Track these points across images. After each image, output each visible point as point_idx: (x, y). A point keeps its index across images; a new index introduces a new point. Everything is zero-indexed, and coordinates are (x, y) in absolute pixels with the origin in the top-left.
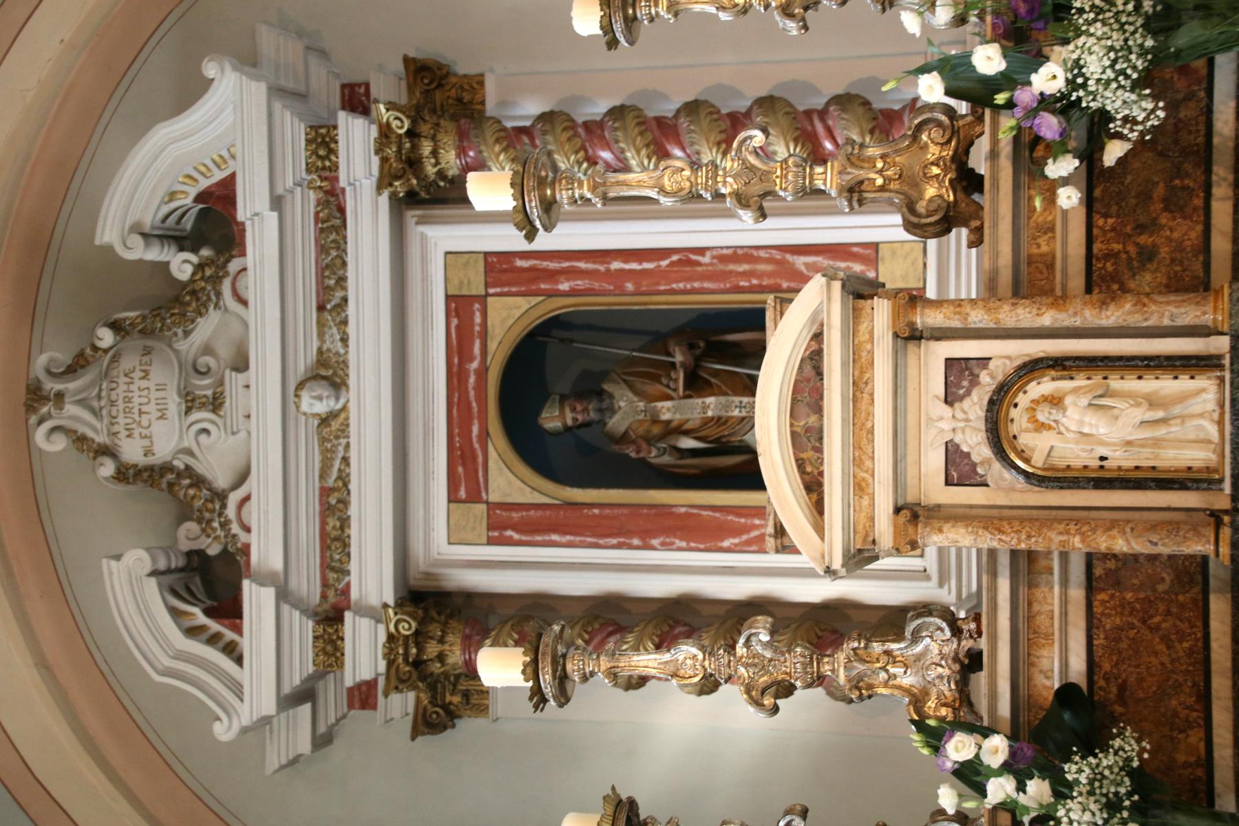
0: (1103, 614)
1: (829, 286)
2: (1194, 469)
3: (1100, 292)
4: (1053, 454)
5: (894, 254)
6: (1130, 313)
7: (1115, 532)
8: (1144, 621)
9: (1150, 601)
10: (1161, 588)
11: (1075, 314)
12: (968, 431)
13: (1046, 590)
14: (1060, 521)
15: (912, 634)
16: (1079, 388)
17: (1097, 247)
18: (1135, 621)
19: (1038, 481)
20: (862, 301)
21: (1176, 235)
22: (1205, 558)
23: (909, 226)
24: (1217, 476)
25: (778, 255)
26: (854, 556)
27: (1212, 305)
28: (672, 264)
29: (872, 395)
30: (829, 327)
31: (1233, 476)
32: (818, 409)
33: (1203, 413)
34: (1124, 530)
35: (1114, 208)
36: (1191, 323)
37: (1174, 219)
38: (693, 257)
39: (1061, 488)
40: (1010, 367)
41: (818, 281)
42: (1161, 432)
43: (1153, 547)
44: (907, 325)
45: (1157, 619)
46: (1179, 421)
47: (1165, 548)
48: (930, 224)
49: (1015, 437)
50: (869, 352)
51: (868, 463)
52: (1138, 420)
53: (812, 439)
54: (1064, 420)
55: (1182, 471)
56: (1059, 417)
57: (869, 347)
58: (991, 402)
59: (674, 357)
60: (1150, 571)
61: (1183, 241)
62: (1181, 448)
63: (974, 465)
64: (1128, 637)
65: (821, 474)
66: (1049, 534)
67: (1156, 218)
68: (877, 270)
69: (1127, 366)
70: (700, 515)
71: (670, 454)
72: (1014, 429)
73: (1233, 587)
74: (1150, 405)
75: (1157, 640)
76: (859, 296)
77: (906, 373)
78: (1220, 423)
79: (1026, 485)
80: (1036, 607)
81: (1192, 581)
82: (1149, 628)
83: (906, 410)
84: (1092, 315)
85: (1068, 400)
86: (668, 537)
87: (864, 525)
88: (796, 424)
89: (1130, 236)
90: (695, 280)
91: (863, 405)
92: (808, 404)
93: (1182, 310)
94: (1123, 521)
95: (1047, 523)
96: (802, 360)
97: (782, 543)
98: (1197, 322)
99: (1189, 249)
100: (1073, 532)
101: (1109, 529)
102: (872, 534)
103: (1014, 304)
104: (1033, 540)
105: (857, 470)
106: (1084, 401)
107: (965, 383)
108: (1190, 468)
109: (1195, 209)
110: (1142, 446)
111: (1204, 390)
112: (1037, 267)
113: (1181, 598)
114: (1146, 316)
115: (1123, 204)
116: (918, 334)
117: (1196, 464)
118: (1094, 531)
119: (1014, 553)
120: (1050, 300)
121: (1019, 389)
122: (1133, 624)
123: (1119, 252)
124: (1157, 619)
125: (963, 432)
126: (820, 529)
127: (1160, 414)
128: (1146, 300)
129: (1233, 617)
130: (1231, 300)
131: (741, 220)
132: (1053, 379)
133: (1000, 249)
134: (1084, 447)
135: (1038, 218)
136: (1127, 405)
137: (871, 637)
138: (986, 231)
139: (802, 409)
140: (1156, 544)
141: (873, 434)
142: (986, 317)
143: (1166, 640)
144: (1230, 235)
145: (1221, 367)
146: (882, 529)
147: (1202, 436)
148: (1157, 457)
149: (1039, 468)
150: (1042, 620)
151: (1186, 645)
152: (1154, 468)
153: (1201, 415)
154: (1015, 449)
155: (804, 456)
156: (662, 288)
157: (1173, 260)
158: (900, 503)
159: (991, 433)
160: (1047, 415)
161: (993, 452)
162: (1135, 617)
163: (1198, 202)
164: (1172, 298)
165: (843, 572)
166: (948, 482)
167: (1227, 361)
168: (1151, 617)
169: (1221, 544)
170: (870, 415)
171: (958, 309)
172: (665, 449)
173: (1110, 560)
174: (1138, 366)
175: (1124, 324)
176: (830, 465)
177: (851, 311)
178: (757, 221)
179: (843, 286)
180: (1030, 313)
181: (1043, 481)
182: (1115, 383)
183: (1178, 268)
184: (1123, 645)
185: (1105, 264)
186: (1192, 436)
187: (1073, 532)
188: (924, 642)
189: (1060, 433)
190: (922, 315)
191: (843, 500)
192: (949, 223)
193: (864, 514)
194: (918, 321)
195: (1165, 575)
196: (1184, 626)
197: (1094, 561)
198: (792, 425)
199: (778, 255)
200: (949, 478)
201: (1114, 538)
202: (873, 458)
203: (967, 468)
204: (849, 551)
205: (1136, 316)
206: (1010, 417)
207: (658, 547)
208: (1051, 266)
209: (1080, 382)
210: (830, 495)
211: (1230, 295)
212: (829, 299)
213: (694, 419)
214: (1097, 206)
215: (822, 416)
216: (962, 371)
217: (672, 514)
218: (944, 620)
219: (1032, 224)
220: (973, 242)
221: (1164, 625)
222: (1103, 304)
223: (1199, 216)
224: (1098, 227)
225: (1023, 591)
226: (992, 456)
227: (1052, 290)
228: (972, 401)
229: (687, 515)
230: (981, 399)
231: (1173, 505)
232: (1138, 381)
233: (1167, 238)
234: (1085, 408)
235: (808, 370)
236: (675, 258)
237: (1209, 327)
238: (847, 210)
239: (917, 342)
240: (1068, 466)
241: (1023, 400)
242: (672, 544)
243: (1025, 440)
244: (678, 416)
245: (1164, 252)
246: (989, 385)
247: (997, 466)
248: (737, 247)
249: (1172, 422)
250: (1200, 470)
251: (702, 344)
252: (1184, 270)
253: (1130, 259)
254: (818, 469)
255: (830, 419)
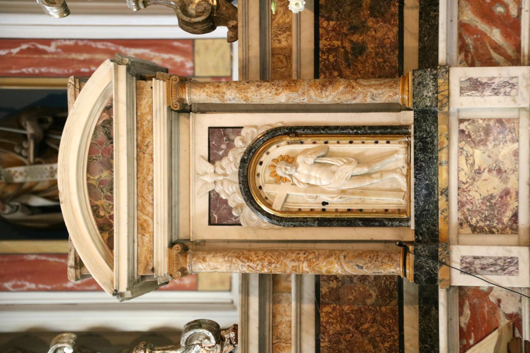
0: (327, 322)
1: (116, 70)
2: (390, 211)
3: (325, 78)
4: (288, 200)
5: (207, 48)
6: (343, 93)
7: (332, 259)
8: (357, 328)
9: (361, 312)
10: (369, 302)
11: (303, 93)
12: (225, 183)
13: (286, 305)
14: (293, 251)
15: (186, 343)
16: (308, 150)
17: (322, 43)
18: (351, 328)
19: (278, 221)
20: (144, 82)
21: (379, 35)
22: (400, 279)
23: (184, 25)
24: (405, 217)
25: (112, 47)
26: (138, 281)
27: (401, 87)
28: (22, 52)
29: (152, 155)
30: (117, 102)
31: (415, 216)
32: (109, 167)
33: (396, 169)
34: (339, 257)
35: (334, 14)
36: (387, 102)
37: (378, 22)
38: (40, 47)
39: (295, 226)
40: (258, 134)
41: (107, 66)
42: (366, 183)
43: (360, 270)
44: (178, 101)
45: (366, 326)
46: (378, 175)
47: (370, 271)
48: (198, 23)
49: (260, 187)
50: (149, 122)
51: (149, 208)
52: (349, 174)
53: (104, 190)
54: (296, 175)
55: (381, 213)
56: (293, 172)
57: (149, 118)
58: (243, 161)
59: (25, 130)
60: (361, 289)
61: (384, 39)
62: (380, 195)
63: (230, 209)
64: (345, 340)
65: (112, 217)
66: (285, 261)
67: (365, 22)
68: (193, 61)
69: (342, 134)
70: (48, 261)
71: (22, 211)
72: (260, 181)
73: (420, 300)
74: (358, 163)
75: (367, 341)
76: (142, 78)
77: (178, 139)
78: (408, 176)
79: (269, 224)
80: (279, 319)
81: (391, 296)
82: (361, 332)
83: (178, 166)
84: (316, 95)
85: (299, 160)
86: (20, 280)
87: (146, 257)
88: (92, 178)
89: (346, 35)
90: (43, 66)
91: (145, 163)
92: (102, 163)
93: (380, 91)
94: (339, 250)
95: (284, 253)
96: (96, 128)
97: (81, 273)
98: (391, 100)
99: (388, 45)
100: (302, 259)
101: (329, 257)
102: (151, 264)
103: (258, 86)
104: (273, 266)
105: (140, 214)
106: (311, 161)
107: (224, 146)
108: (386, 210)
109: (392, 15)
110: (353, 194)
111: (396, 152)
112: (279, 58)
113: (383, 309)
114: (355, 95)
115: (341, 10)
116: (188, 108)
117: (391, 207)
118: (317, 258)
119: (262, 277)
120: (285, 83)
121: (263, 151)
122: (349, 330)
123: (339, 47)
124: (366, 326)
125: (222, 184)
126: (110, 261)
127: (365, 170)
128: (354, 84)
129: (420, 323)
130: (414, 84)
131: (49, 15)
132: (288, 143)
133: (250, 43)
134: (310, 195)
135: (280, 20)
136: (342, 163)
137: (154, 347)
138: (240, 29)
139: (97, 166)
140: (362, 268)
141: (152, 185)
142: (238, 96)
143: (372, 341)
144: (418, 35)
145: (408, 134)
146: (159, 259)
147: (395, 186)
148: (363, 202)
149: (278, 211)
150: (283, 328)
151: (387, 345)
152: (361, 210)
153: (394, 171)
154: (260, 197)
155: (98, 203)
156: (14, 72)
157: (377, 54)
158: (174, 239)
159: (243, 184)
160: (284, 170)
161: (244, 199)
162: (351, 324)
163: (395, 10)
164: (373, 82)
165: (128, 294)
166: (211, 223)
167: (412, 130)
168: (362, 324)
169: (407, 267)
170: (150, 170)
171: (217, 89)
172: (18, 206)
173: (333, 281)
174: (350, 134)
175: (339, 102)
176: (118, 210)
177: (135, 89)
178: (62, 16)
179: (128, 70)
180: (270, 92)
181: (281, 221)
182: (333, 147)
183: (380, 60)
184: (342, 346)
185: (328, 56)
186: (388, 186)
187: (302, 259)
188: (195, 349)
189: (293, 184)
190: (190, 94)
191: (128, 237)
192: (213, 21)
193: (145, 248)
194: (187, 98)
195: (371, 292)
196: (385, 330)
197: (321, 282)
198: (88, 179)
199: (112, 47)
200: (212, 219)
201: (332, 263)
202: (153, 204)
203: (225, 211)
204: (133, 277)
205: (348, 95)
206: (257, 173)
207: (10, 289)
208: (289, 57)
209: (308, 145)
210: (119, 234)
211: (413, 80)
212: (117, 79)
213: (43, 182)
214: (322, 11)
215: (113, 172)
216: (221, 137)
217: (23, 261)
218: (210, 331)
219: (275, 24)
220: (231, 38)
221: (371, 330)
222: (324, 86)
223: (395, 20)
224: (323, 28)
225: (269, 306)
226: (244, 202)
227: (290, 76)
228: (229, 160)
229: (37, 261)
230: (235, 159)
231: (375, 238)
232: (350, 145)
233: (372, 36)
234: (311, 165)
235: (101, 136)
236: (24, 47)
237: (398, 104)
238: (135, 10)
239: (187, 114)
240: (300, 210)
241: (266, 159)
242: (23, 286)
243: (268, 190)
244: (29, 179)
245: (371, 47)
246: (241, 148)
247: (247, 210)
248: (78, 39)
249: (374, 176)
250: (393, 212)
251: (50, 119)
252: (385, 62)
253: (346, 52)
254: (109, 213)
255: (118, 173)
